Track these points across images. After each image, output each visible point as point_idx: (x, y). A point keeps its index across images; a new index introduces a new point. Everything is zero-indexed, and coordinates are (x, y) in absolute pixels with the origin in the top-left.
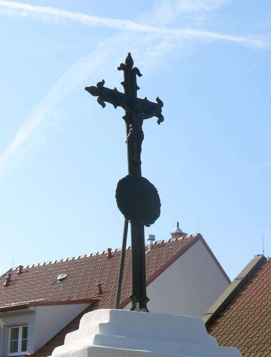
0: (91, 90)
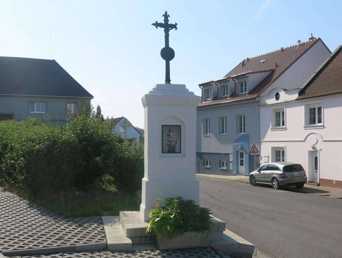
0: (153, 24)
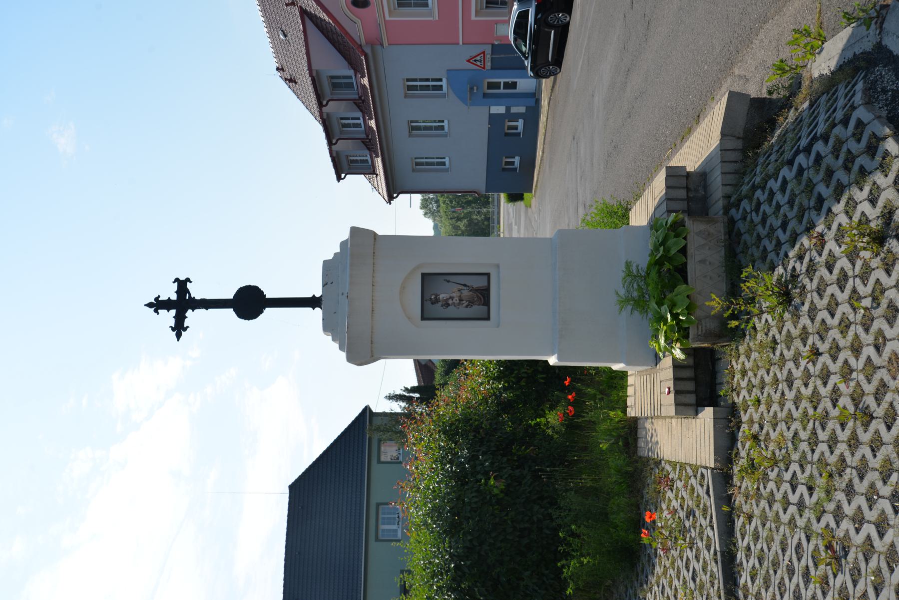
0: (179, 336)
